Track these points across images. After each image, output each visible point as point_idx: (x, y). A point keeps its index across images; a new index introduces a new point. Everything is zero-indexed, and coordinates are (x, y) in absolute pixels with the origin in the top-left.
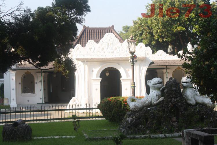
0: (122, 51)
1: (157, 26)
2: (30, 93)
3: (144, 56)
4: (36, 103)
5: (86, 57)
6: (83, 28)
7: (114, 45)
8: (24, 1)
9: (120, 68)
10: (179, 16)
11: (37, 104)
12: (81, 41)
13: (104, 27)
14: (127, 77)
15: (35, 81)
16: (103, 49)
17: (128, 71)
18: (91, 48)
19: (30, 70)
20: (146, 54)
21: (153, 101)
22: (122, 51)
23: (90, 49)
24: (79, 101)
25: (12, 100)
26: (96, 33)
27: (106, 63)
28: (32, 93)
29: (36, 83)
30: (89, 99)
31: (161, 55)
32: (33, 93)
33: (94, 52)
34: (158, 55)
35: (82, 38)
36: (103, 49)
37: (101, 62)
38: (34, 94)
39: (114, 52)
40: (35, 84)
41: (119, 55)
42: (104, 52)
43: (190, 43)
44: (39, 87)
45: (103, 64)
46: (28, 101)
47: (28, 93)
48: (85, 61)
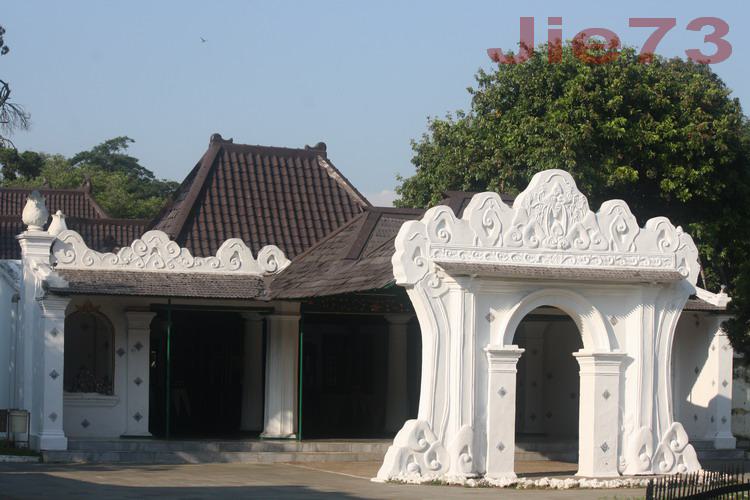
0: (598, 243)
1: (554, 157)
2: (95, 391)
3: (670, 267)
4: (118, 435)
5: (470, 259)
6: (207, 148)
7: (571, 219)
8: (527, 24)
9: (587, 312)
10: (627, 127)
11: (123, 437)
12: (210, 192)
13: (248, 143)
14: (612, 348)
15: (119, 344)
16: (531, 232)
17: (614, 324)
18: (490, 224)
19: (283, 303)
20: (679, 261)
21: (739, 432)
22: (598, 243)
23: (485, 227)
24: (436, 439)
25: (47, 421)
26: (263, 166)
27: (541, 288)
28: (101, 393)
29: (121, 353)
30: (474, 429)
31: (155, 249)
32: (107, 394)
33: (500, 242)
34: (144, 248)
35: (214, 184)
36: (531, 232)
37: (521, 283)
38: (111, 397)
39: (569, 247)
40: (117, 355)
41: (588, 260)
42: (536, 243)
43: (59, 213)
44: (133, 374)
45: (529, 292)
46: (85, 424)
47: (86, 392)
48: (468, 276)
